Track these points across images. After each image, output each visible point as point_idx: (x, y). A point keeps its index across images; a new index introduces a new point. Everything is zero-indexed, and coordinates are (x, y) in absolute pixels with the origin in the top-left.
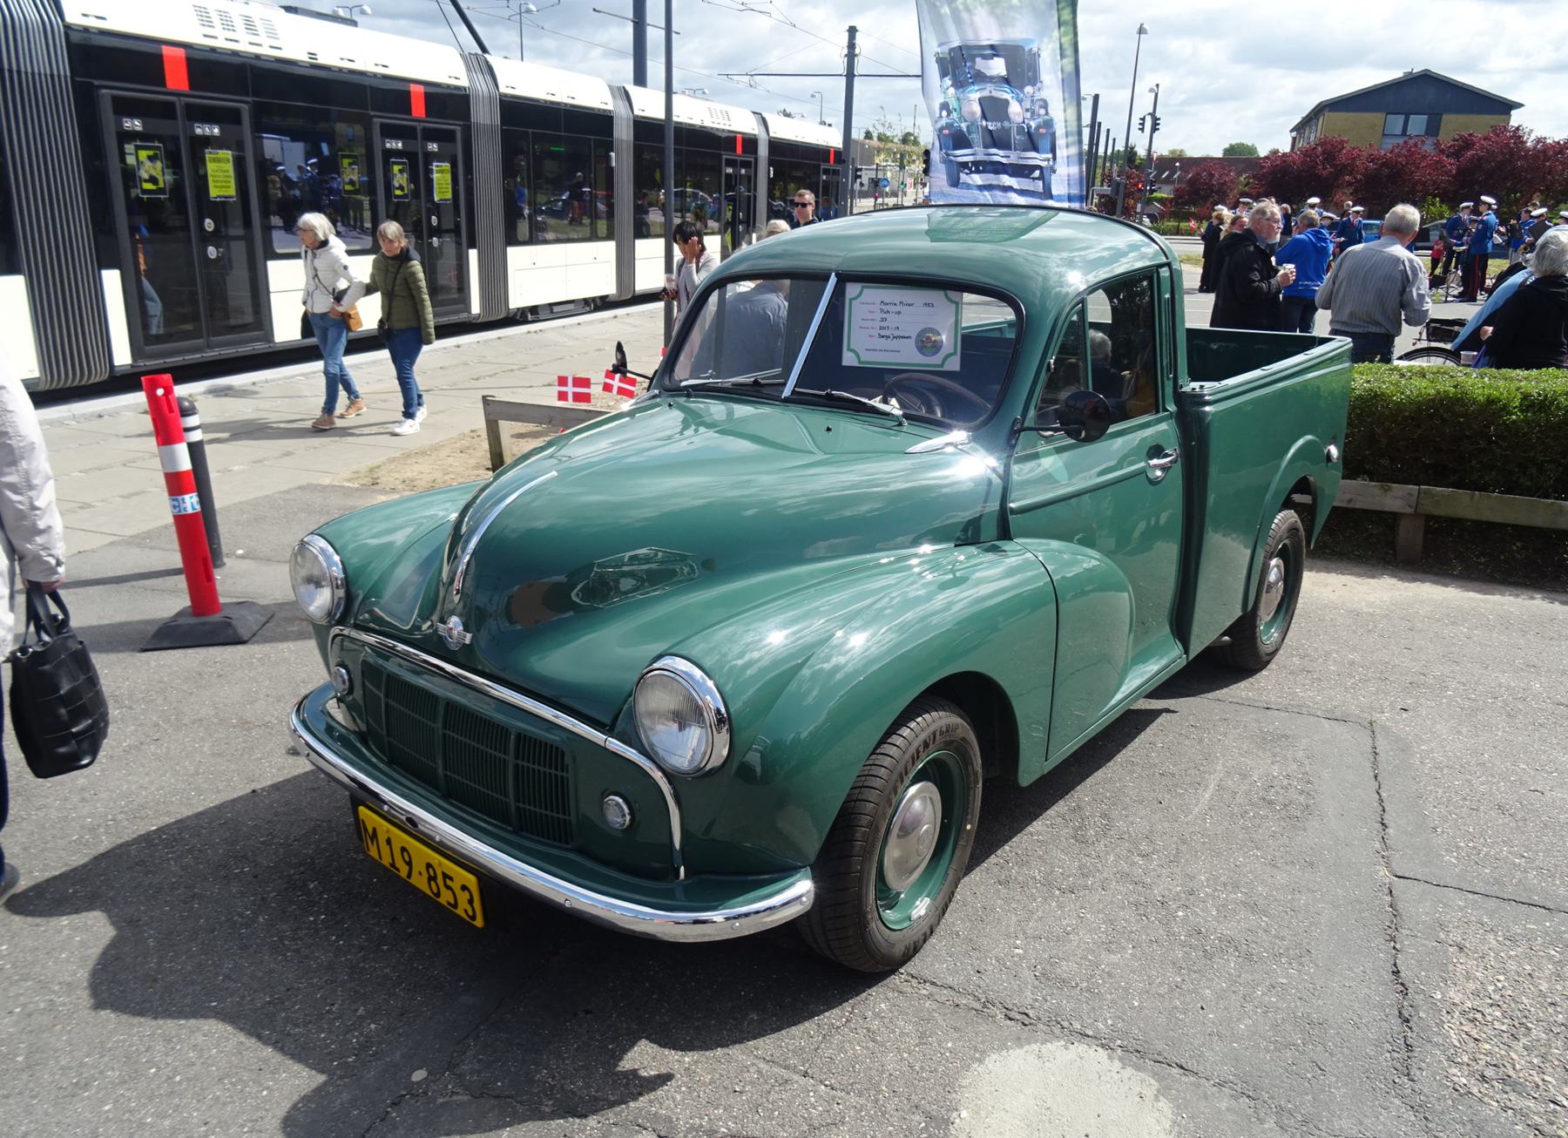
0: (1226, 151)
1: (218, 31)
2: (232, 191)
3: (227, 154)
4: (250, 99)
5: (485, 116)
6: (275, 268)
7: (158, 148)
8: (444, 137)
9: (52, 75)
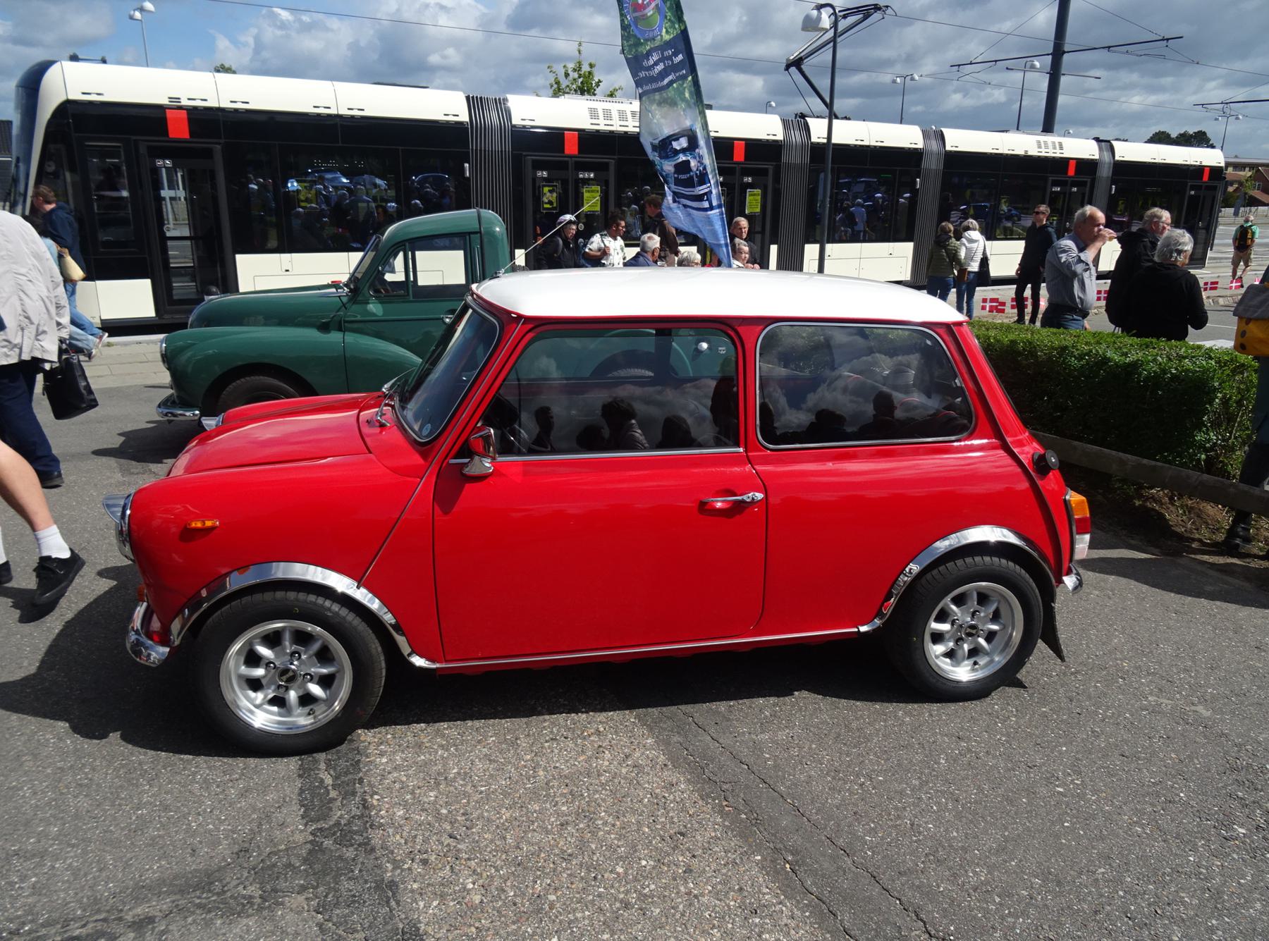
0: (103, 736)
1: (1043, 150)
2: (758, 210)
3: (758, 191)
4: (616, 157)
5: (1105, 172)
6: (772, 246)
7: (556, 186)
8: (758, 173)
9: (502, 151)
